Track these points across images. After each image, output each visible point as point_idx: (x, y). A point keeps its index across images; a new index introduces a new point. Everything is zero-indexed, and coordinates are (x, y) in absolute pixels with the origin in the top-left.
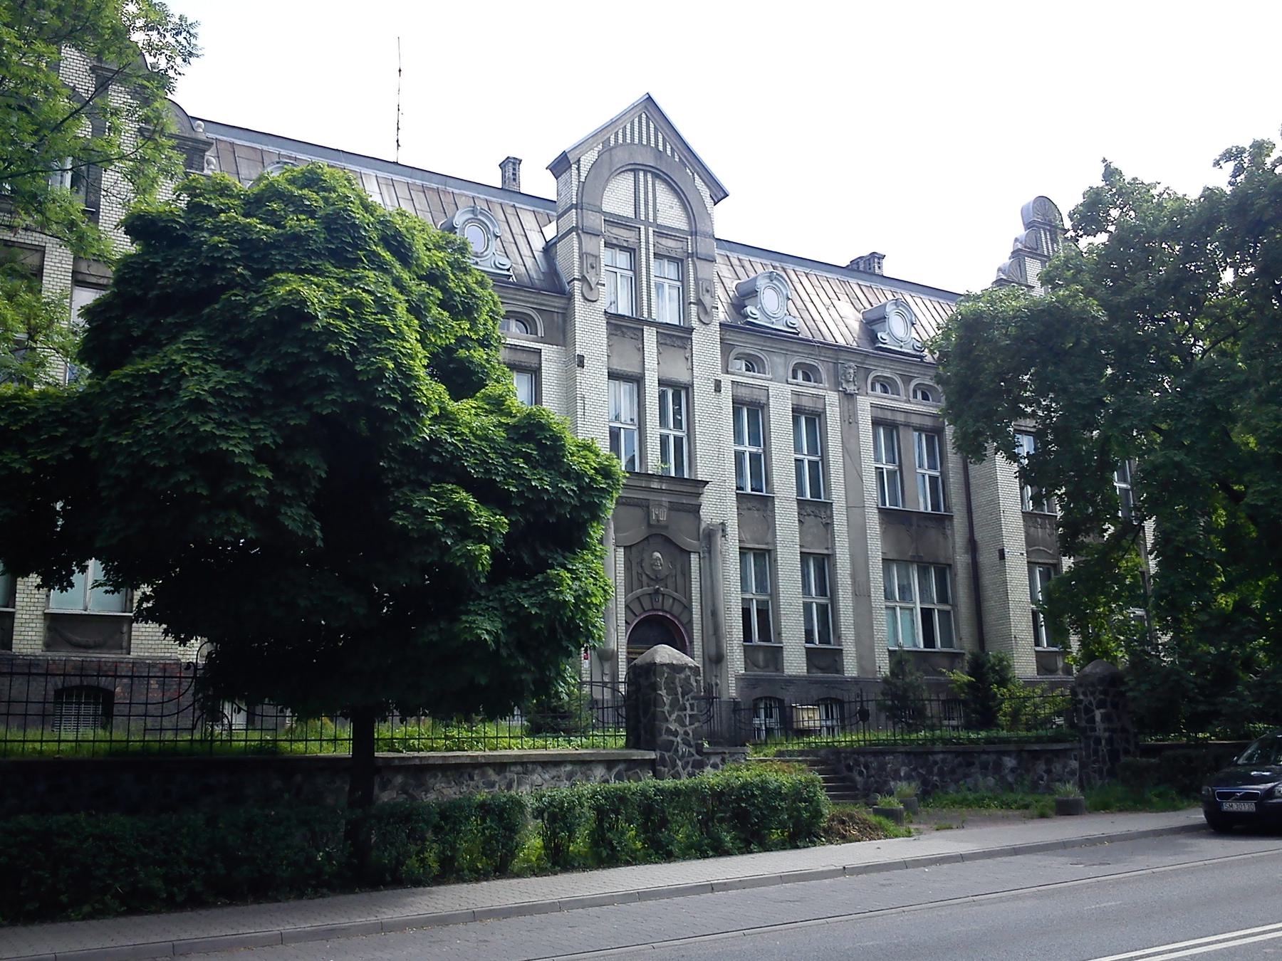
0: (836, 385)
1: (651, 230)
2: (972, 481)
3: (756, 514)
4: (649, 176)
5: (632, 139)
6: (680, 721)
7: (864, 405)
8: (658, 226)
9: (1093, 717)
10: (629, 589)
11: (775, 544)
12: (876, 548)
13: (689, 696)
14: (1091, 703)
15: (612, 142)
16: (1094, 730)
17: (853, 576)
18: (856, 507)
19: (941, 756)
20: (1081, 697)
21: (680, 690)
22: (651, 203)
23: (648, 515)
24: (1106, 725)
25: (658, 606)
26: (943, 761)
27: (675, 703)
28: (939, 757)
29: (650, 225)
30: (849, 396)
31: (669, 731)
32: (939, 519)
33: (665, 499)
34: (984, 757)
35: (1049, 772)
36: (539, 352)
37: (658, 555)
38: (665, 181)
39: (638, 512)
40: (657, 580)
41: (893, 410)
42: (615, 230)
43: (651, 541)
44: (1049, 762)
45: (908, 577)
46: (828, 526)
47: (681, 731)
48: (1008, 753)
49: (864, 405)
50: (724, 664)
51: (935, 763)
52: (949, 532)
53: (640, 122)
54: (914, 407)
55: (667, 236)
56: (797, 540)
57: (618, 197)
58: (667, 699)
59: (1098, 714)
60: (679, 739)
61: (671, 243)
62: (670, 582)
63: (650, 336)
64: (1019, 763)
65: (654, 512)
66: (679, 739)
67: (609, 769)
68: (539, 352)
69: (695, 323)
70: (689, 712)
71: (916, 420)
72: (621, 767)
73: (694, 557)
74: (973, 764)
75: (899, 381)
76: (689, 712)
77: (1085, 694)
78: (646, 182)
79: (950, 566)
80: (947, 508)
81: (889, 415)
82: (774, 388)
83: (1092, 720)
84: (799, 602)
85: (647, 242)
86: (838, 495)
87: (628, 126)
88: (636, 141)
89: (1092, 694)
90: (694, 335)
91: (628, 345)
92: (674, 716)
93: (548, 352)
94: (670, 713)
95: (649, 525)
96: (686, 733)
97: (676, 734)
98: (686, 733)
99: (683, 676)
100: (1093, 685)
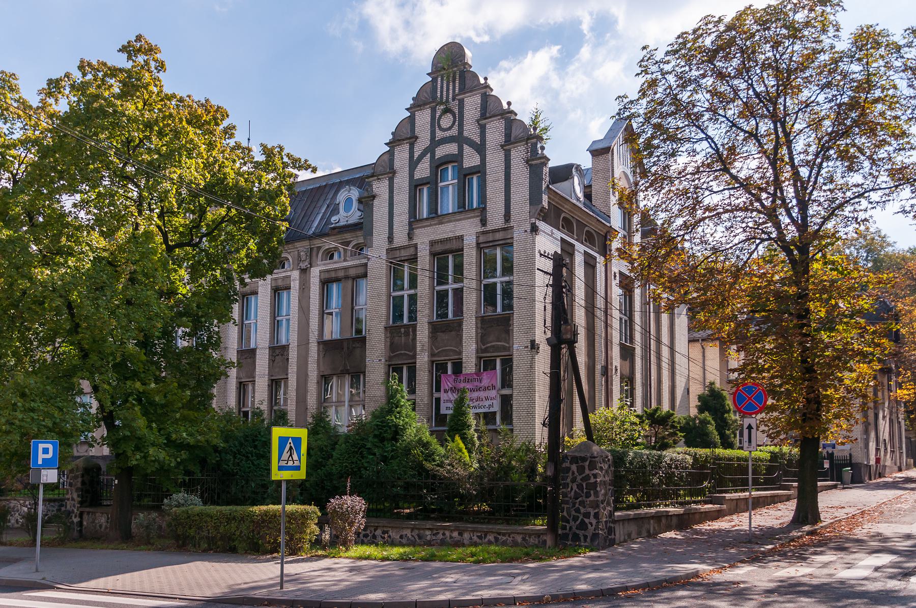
7: (315, 273)
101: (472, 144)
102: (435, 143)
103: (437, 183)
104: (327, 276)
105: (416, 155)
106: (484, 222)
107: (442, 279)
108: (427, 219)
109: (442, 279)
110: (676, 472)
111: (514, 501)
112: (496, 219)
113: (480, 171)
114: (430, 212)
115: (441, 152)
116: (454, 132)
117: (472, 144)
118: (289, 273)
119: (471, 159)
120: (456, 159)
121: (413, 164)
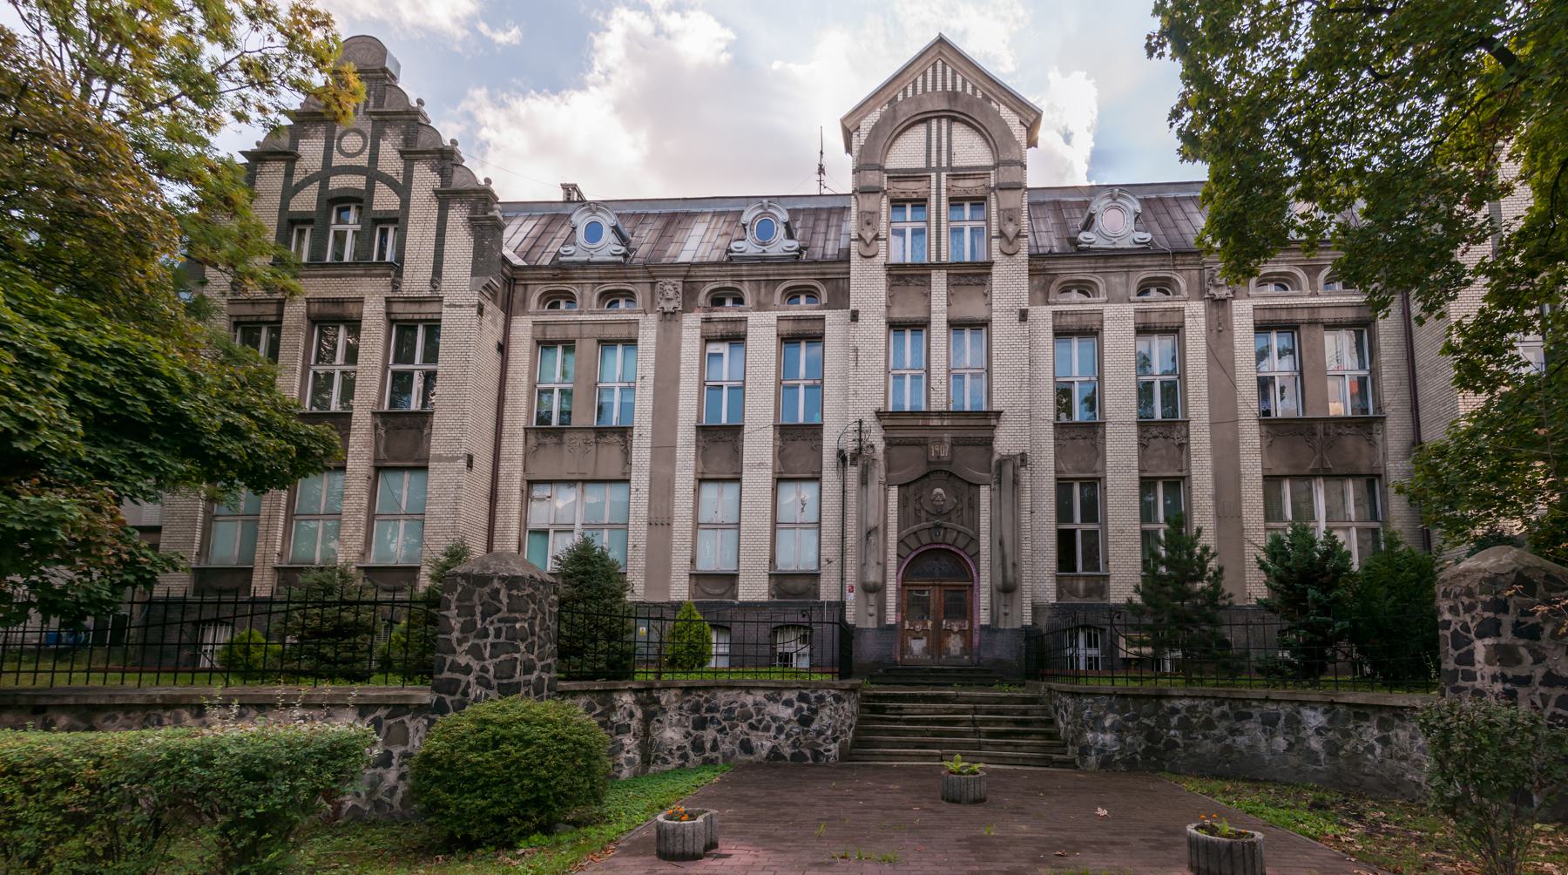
0: (1201, 294)
1: (944, 175)
2: (1419, 372)
3: (1081, 442)
4: (944, 123)
5: (934, 87)
6: (476, 652)
7: (1243, 312)
8: (952, 169)
9: (1471, 653)
10: (902, 524)
11: (1104, 470)
12: (1252, 465)
13: (495, 617)
14: (1466, 628)
15: (900, 97)
16: (1471, 676)
17: (1217, 497)
18: (1225, 419)
19: (1186, 702)
20: (1447, 616)
21: (478, 609)
22: (944, 148)
23: (927, 452)
24: (1497, 669)
25: (940, 539)
26: (1191, 710)
27: (468, 628)
28: (1178, 704)
29: (944, 170)
30: (1220, 303)
31: (455, 667)
32: (1365, 424)
33: (947, 436)
34: (1271, 707)
35: (1385, 741)
36: (822, 319)
37: (939, 490)
38: (964, 122)
39: (917, 450)
40: (939, 514)
41: (1289, 308)
42: (903, 185)
43: (932, 477)
44: (1384, 725)
45: (1310, 500)
46: (1183, 446)
47: (476, 665)
48: (1312, 705)
49: (1243, 312)
50: (1017, 595)
51: (1174, 711)
52: (1378, 438)
53: (935, 71)
54: (1325, 300)
55: (964, 177)
56: (1136, 464)
57: (909, 152)
58: (456, 623)
59: (1480, 648)
60: (471, 678)
61: (969, 183)
62: (953, 517)
63: (939, 281)
64: (1330, 721)
65: (934, 450)
66: (471, 678)
67: (362, 715)
68: (822, 319)
69: (996, 256)
70: (491, 639)
71: (1327, 315)
72: (381, 713)
73: (984, 492)
74: (1250, 716)
75: (1301, 274)
76: (491, 639)
77: (1453, 610)
78: (939, 129)
79: (1379, 476)
80: (1378, 408)
81: (1284, 316)
82: (1109, 310)
83: (1468, 659)
84: (1135, 528)
85: (939, 188)
86: (1198, 407)
87: (920, 79)
88: (929, 89)
89: (1469, 609)
90: (994, 270)
91: (913, 292)
92: (466, 646)
93: (831, 316)
94: (460, 642)
95: (929, 463)
96: (484, 669)
97: (467, 670)
98: (484, 669)
99: (487, 589)
100: (1469, 593)
101: (390, 182)
102: (328, 170)
103: (327, 226)
104: (1268, 316)
105: (296, 179)
106: (396, 286)
107: (404, 354)
108: (307, 265)
109: (404, 354)
110: (266, 464)
111: (177, 292)
112: (416, 279)
113: (397, 220)
114: (311, 258)
115: (337, 183)
116: (362, 160)
117: (390, 182)
118: (1181, 304)
119: (385, 200)
120: (358, 200)
121: (289, 191)
